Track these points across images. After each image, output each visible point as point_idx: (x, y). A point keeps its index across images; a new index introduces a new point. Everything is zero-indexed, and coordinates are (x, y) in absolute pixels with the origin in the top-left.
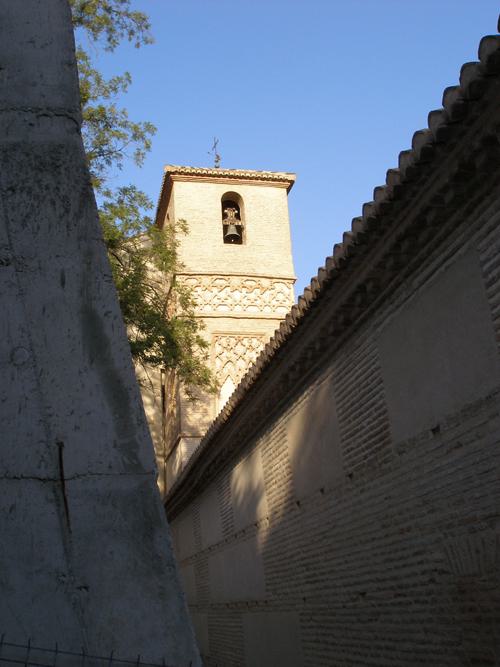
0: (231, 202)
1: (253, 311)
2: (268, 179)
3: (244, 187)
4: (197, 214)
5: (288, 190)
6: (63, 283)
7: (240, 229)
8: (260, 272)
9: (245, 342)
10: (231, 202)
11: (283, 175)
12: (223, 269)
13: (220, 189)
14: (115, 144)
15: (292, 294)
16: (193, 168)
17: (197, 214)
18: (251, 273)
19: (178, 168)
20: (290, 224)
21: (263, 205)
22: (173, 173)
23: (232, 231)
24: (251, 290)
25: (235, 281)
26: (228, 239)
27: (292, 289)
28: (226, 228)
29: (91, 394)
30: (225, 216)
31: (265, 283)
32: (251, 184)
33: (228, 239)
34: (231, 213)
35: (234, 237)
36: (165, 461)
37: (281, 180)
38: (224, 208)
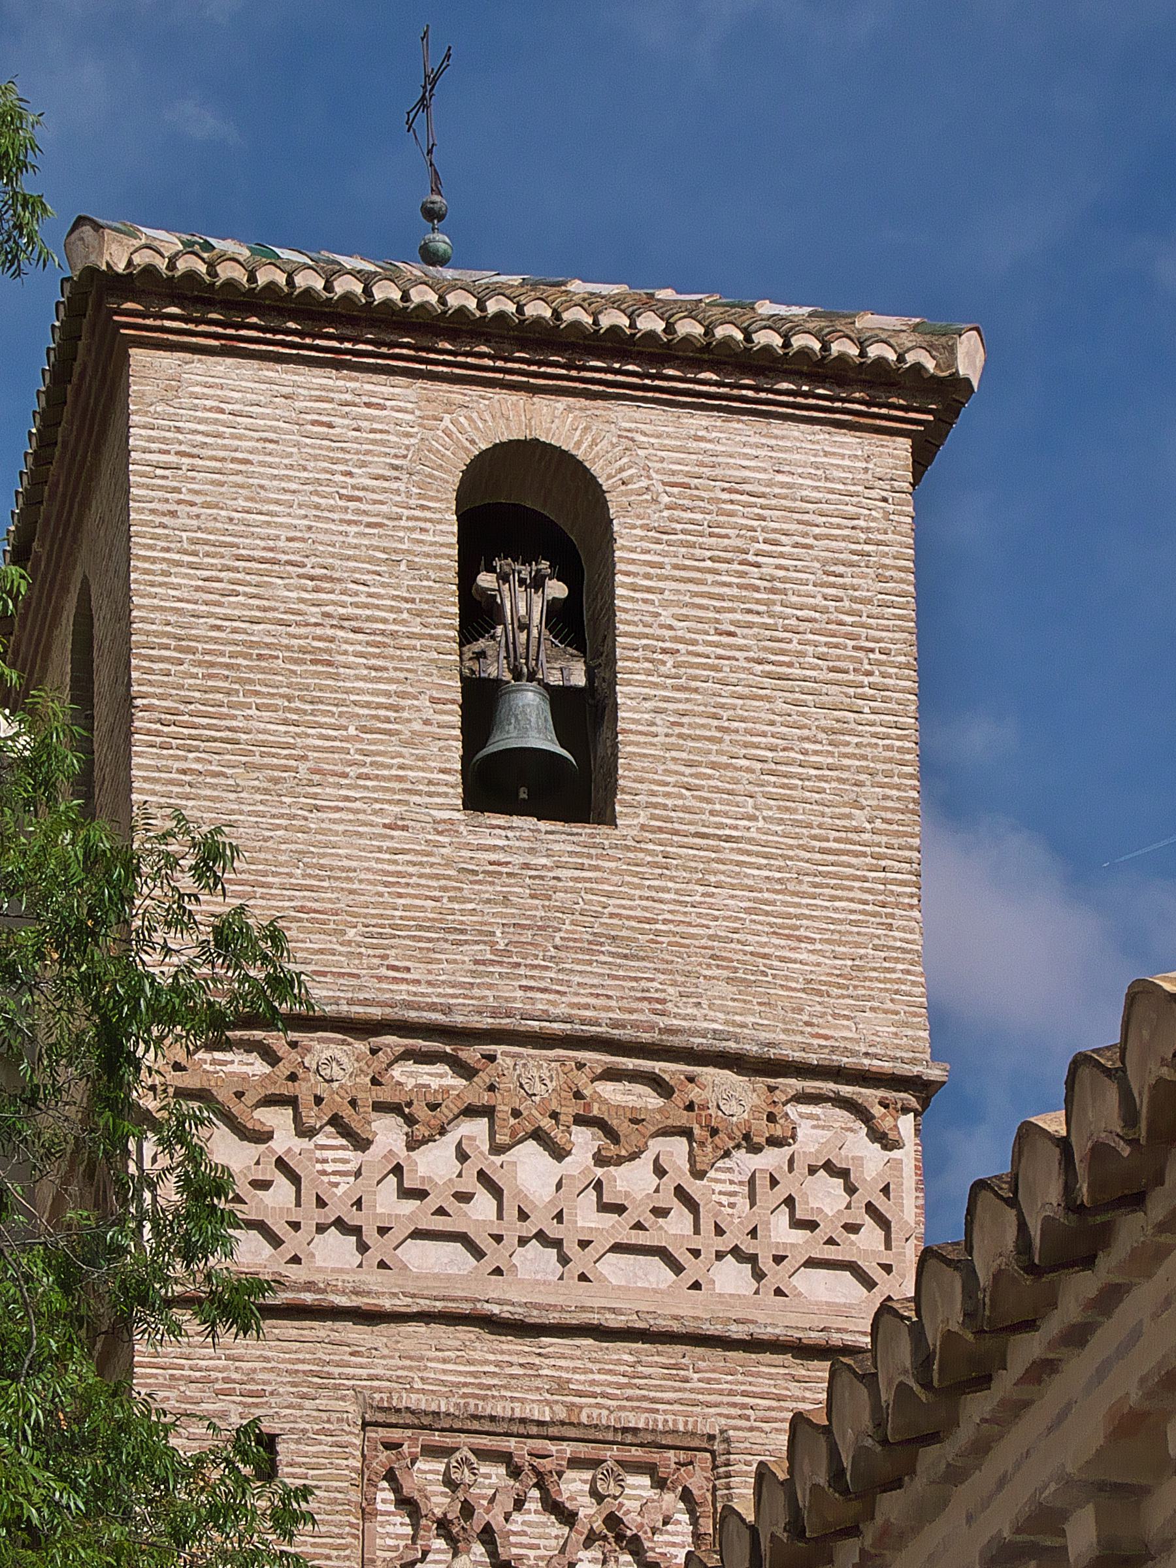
0: (528, 524)
1: (632, 1286)
3: (624, 415)
4: (286, 592)
5: (921, 461)
7: (586, 714)
8: (704, 1018)
9: (573, 1486)
10: (528, 524)
11: (885, 335)
15: (909, 1178)
16: (264, 253)
18: (640, 1022)
21: (761, 549)
23: (530, 725)
25: (535, 1075)
26: (496, 782)
27: (908, 1155)
28: (481, 703)
29: (353, 1103)
30: (478, 615)
31: (733, 1097)
33: (496, 782)
34: (527, 600)
35: (546, 770)
36: (100, 1373)
38: (472, 556)
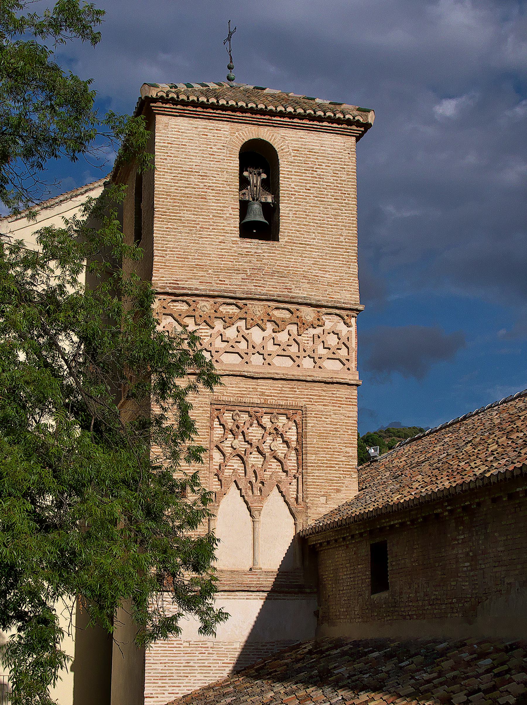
0: (258, 159)
2: (320, 119)
3: (282, 132)
4: (194, 179)
6: (271, 355)
7: (272, 211)
8: (302, 292)
10: (258, 159)
12: (234, 284)
13: (234, 135)
14: (95, 30)
17: (194, 179)
19: (163, 89)
20: (153, 208)
21: (317, 165)
22: (155, 100)
23: (256, 214)
24: (279, 326)
25: (257, 309)
26: (247, 230)
28: (244, 207)
30: (244, 183)
32: (294, 127)
33: (247, 230)
34: (256, 179)
35: (261, 225)
37: (349, 122)
38: (243, 167)
